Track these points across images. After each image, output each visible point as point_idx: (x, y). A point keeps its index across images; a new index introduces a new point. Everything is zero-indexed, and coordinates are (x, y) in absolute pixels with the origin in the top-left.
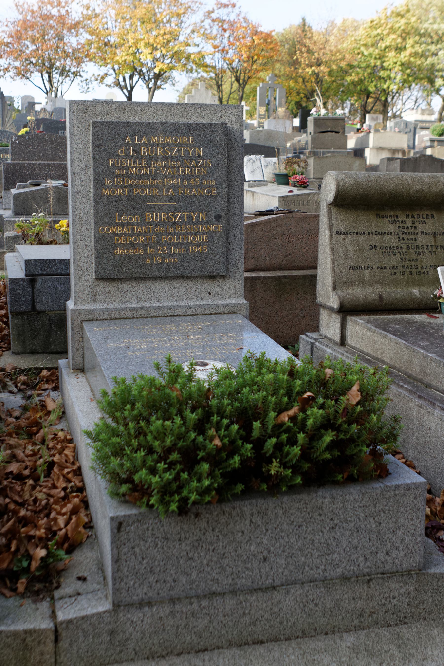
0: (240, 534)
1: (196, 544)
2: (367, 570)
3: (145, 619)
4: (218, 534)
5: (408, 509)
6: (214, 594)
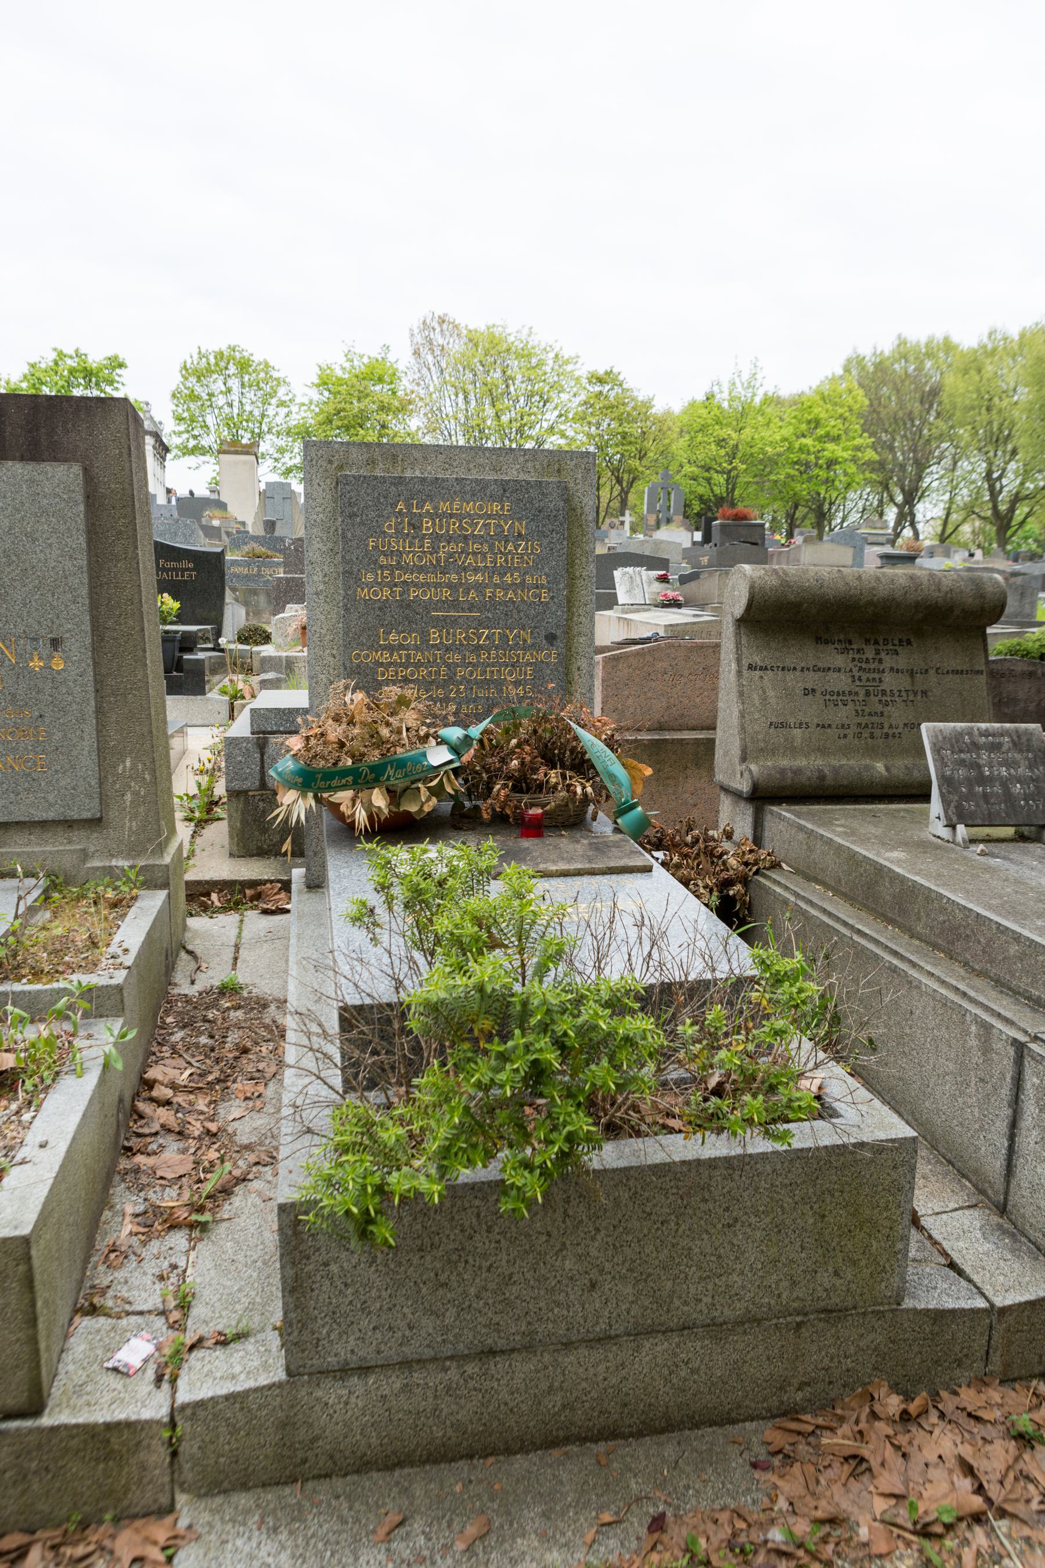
0: (544, 1238)
1: (455, 1257)
2: (795, 1305)
3: (353, 1400)
4: (498, 1237)
5: (880, 1188)
6: (492, 1352)
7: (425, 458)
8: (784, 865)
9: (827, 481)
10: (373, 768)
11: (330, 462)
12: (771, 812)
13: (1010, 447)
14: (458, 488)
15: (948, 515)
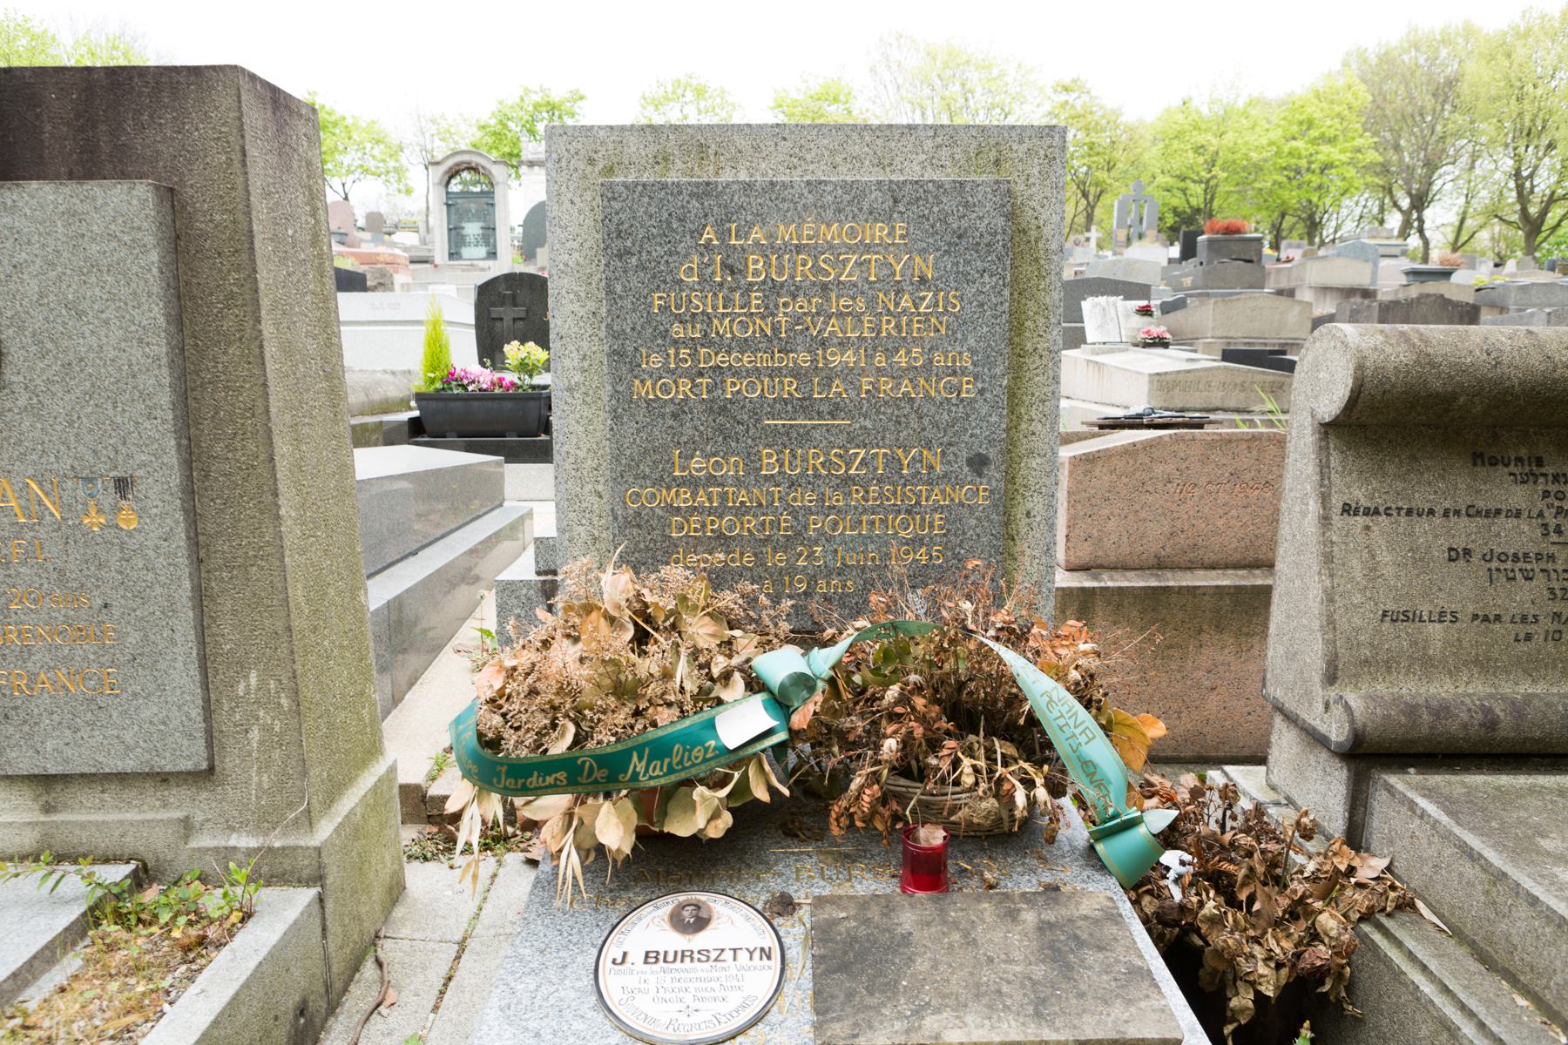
7: (756, 149)
8: (1420, 904)
9: (1320, 187)
10: (602, 760)
11: (591, 162)
12: (1390, 789)
13: (1545, 141)
14: (811, 199)
15: (1462, 221)
